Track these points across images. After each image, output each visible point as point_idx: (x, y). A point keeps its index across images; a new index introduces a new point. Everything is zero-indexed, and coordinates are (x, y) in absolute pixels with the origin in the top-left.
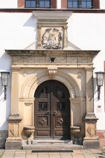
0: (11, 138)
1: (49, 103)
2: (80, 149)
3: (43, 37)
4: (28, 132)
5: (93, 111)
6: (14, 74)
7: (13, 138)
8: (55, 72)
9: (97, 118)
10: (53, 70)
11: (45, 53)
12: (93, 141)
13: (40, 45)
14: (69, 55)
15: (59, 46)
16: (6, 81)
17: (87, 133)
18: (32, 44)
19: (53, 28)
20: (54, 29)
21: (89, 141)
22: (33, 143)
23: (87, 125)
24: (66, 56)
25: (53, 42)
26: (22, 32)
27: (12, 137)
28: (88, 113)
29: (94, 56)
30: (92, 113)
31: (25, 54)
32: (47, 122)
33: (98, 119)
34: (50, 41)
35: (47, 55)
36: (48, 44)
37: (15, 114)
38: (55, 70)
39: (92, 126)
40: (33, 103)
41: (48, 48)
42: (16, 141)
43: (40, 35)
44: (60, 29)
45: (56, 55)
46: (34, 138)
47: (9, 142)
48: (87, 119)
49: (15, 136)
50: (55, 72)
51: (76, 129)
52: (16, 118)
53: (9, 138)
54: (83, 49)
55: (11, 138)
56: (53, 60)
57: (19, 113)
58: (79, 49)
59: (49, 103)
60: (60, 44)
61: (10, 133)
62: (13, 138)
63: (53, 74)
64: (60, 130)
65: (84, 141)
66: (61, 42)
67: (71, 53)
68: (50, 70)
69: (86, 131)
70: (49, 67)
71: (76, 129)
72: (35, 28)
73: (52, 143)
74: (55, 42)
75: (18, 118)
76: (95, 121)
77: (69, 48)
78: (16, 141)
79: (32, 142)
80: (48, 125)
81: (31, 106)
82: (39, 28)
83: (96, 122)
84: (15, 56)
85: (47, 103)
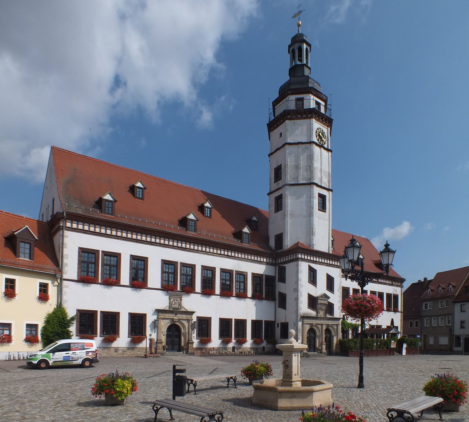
33: (346, 280)
54: (189, 311)
82: (170, 299)
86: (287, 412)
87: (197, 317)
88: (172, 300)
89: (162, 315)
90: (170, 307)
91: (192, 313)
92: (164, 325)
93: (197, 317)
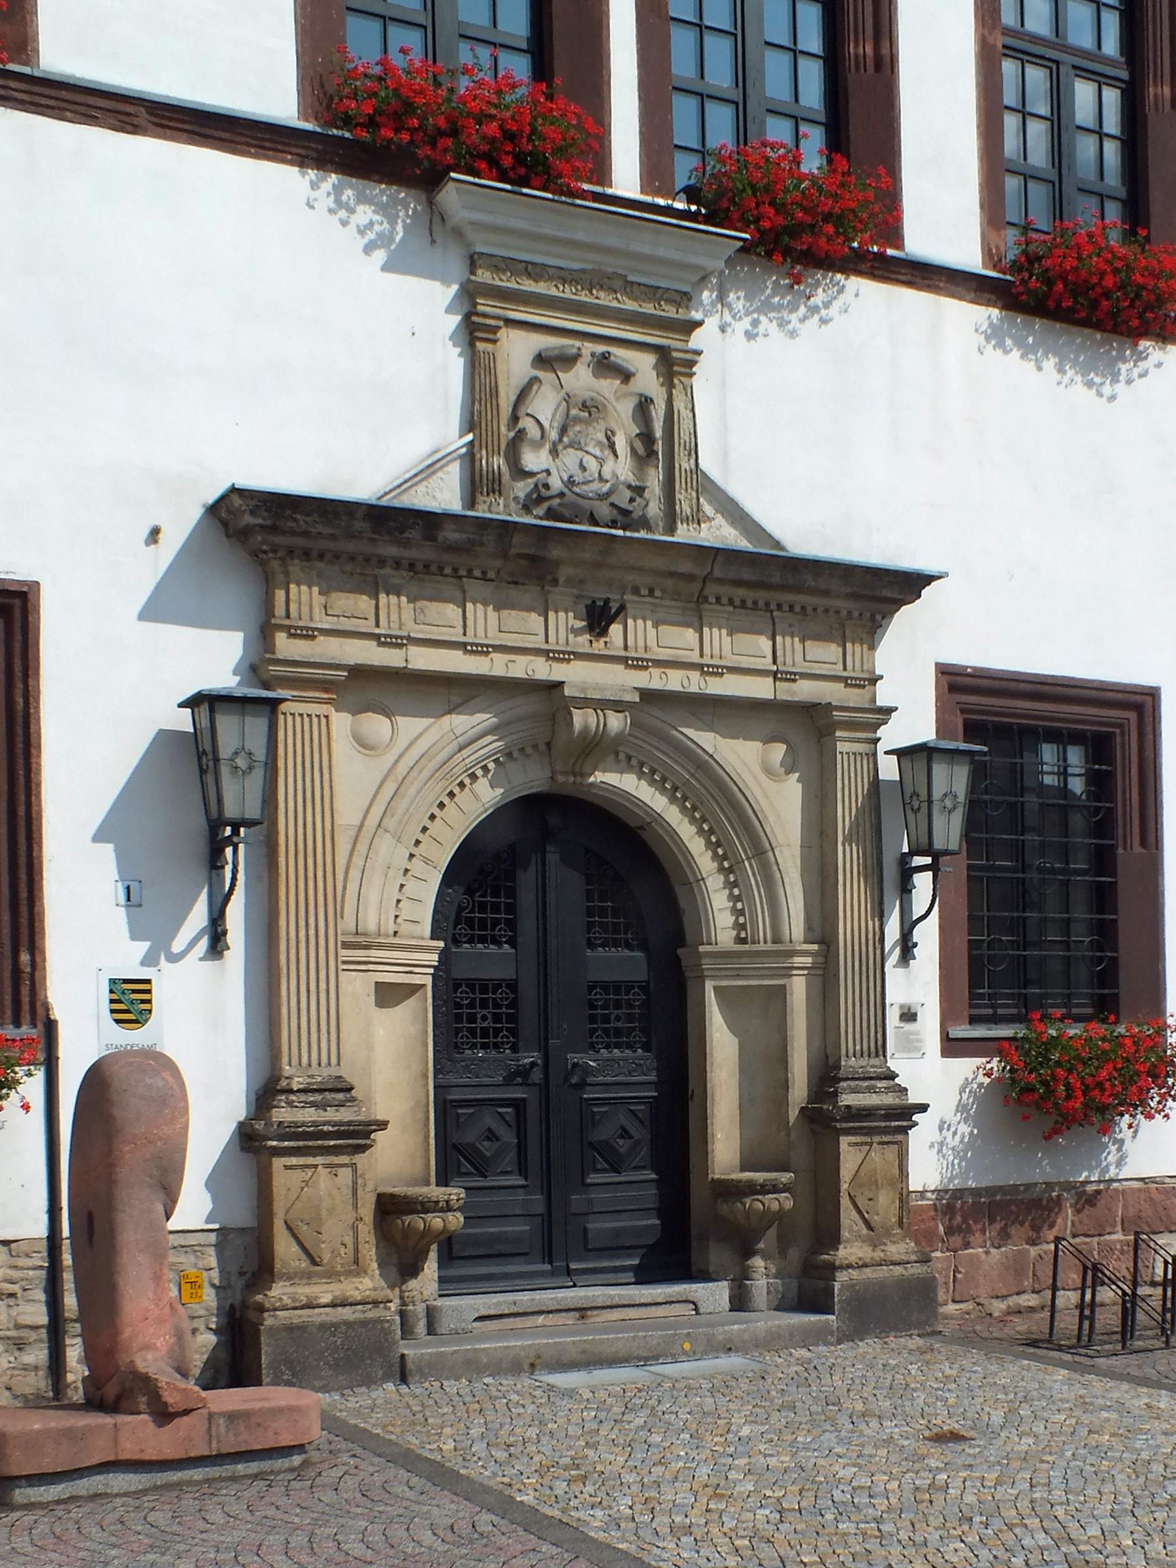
0: (304, 1291)
1: (529, 993)
2: (809, 1338)
3: (515, 418)
4: (748, 1213)
5: (880, 1050)
6: (297, 709)
7: (325, 1293)
8: (616, 722)
9: (913, 1098)
10: (602, 705)
11: (556, 552)
12: (898, 1270)
13: (495, 486)
14: (726, 591)
15: (636, 508)
16: (937, 794)
17: (848, 1217)
18: (430, 469)
19: (589, 348)
20: (605, 356)
21: (868, 1273)
22: (446, 1324)
23: (850, 1155)
24: (702, 599)
25: (592, 464)
26: (342, 353)
27: (307, 1277)
28: (850, 1064)
29: (889, 614)
30: (871, 1065)
31: (391, 551)
32: (522, 1148)
34: (570, 458)
35: (564, 573)
36: (556, 484)
37: (321, 1075)
38: (618, 706)
39: (881, 1157)
40: (428, 981)
41: (551, 514)
42: (346, 1313)
43: (495, 392)
44: (643, 364)
45: (630, 578)
46: (442, 1280)
47: (291, 1329)
48: (841, 1110)
49: (332, 1275)
50: (616, 722)
51: (775, 1188)
52: (331, 1114)
53: (279, 1291)
55: (304, 1291)
56: (598, 619)
57: (345, 1072)
58: (778, 545)
59: (529, 993)
60: (639, 490)
61: (285, 1249)
62: (325, 1293)
63: (595, 748)
64: (622, 1198)
65: (842, 1277)
66: (654, 481)
67: (747, 574)
68: (584, 703)
69: (845, 1202)
70: (576, 676)
71: (775, 1188)
72: (458, 350)
73: (582, 1311)
74: (604, 466)
75: (344, 1115)
76: (904, 1115)
77: (718, 532)
78: (346, 1313)
79: (431, 1315)
80: (523, 1170)
81: (411, 1003)
82: (475, 333)
83: (904, 1131)
84: (306, 555)
85: (513, 986)
86: (492, 1313)
87: (954, 682)
88: (516, 351)
89: (339, 624)
90: (477, 484)
91: (876, 594)
92: (390, 805)
93: (954, 682)
